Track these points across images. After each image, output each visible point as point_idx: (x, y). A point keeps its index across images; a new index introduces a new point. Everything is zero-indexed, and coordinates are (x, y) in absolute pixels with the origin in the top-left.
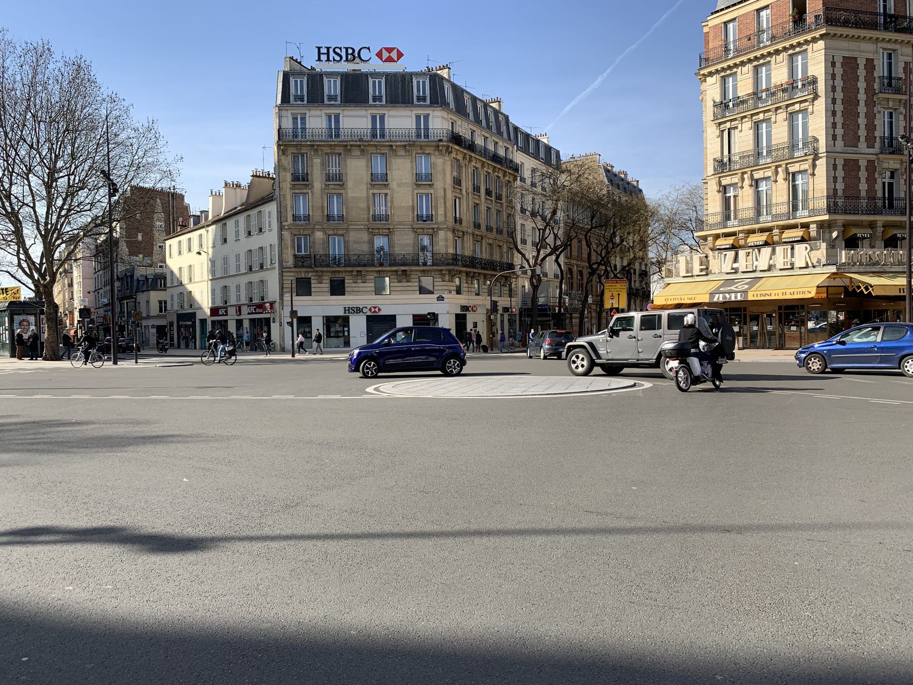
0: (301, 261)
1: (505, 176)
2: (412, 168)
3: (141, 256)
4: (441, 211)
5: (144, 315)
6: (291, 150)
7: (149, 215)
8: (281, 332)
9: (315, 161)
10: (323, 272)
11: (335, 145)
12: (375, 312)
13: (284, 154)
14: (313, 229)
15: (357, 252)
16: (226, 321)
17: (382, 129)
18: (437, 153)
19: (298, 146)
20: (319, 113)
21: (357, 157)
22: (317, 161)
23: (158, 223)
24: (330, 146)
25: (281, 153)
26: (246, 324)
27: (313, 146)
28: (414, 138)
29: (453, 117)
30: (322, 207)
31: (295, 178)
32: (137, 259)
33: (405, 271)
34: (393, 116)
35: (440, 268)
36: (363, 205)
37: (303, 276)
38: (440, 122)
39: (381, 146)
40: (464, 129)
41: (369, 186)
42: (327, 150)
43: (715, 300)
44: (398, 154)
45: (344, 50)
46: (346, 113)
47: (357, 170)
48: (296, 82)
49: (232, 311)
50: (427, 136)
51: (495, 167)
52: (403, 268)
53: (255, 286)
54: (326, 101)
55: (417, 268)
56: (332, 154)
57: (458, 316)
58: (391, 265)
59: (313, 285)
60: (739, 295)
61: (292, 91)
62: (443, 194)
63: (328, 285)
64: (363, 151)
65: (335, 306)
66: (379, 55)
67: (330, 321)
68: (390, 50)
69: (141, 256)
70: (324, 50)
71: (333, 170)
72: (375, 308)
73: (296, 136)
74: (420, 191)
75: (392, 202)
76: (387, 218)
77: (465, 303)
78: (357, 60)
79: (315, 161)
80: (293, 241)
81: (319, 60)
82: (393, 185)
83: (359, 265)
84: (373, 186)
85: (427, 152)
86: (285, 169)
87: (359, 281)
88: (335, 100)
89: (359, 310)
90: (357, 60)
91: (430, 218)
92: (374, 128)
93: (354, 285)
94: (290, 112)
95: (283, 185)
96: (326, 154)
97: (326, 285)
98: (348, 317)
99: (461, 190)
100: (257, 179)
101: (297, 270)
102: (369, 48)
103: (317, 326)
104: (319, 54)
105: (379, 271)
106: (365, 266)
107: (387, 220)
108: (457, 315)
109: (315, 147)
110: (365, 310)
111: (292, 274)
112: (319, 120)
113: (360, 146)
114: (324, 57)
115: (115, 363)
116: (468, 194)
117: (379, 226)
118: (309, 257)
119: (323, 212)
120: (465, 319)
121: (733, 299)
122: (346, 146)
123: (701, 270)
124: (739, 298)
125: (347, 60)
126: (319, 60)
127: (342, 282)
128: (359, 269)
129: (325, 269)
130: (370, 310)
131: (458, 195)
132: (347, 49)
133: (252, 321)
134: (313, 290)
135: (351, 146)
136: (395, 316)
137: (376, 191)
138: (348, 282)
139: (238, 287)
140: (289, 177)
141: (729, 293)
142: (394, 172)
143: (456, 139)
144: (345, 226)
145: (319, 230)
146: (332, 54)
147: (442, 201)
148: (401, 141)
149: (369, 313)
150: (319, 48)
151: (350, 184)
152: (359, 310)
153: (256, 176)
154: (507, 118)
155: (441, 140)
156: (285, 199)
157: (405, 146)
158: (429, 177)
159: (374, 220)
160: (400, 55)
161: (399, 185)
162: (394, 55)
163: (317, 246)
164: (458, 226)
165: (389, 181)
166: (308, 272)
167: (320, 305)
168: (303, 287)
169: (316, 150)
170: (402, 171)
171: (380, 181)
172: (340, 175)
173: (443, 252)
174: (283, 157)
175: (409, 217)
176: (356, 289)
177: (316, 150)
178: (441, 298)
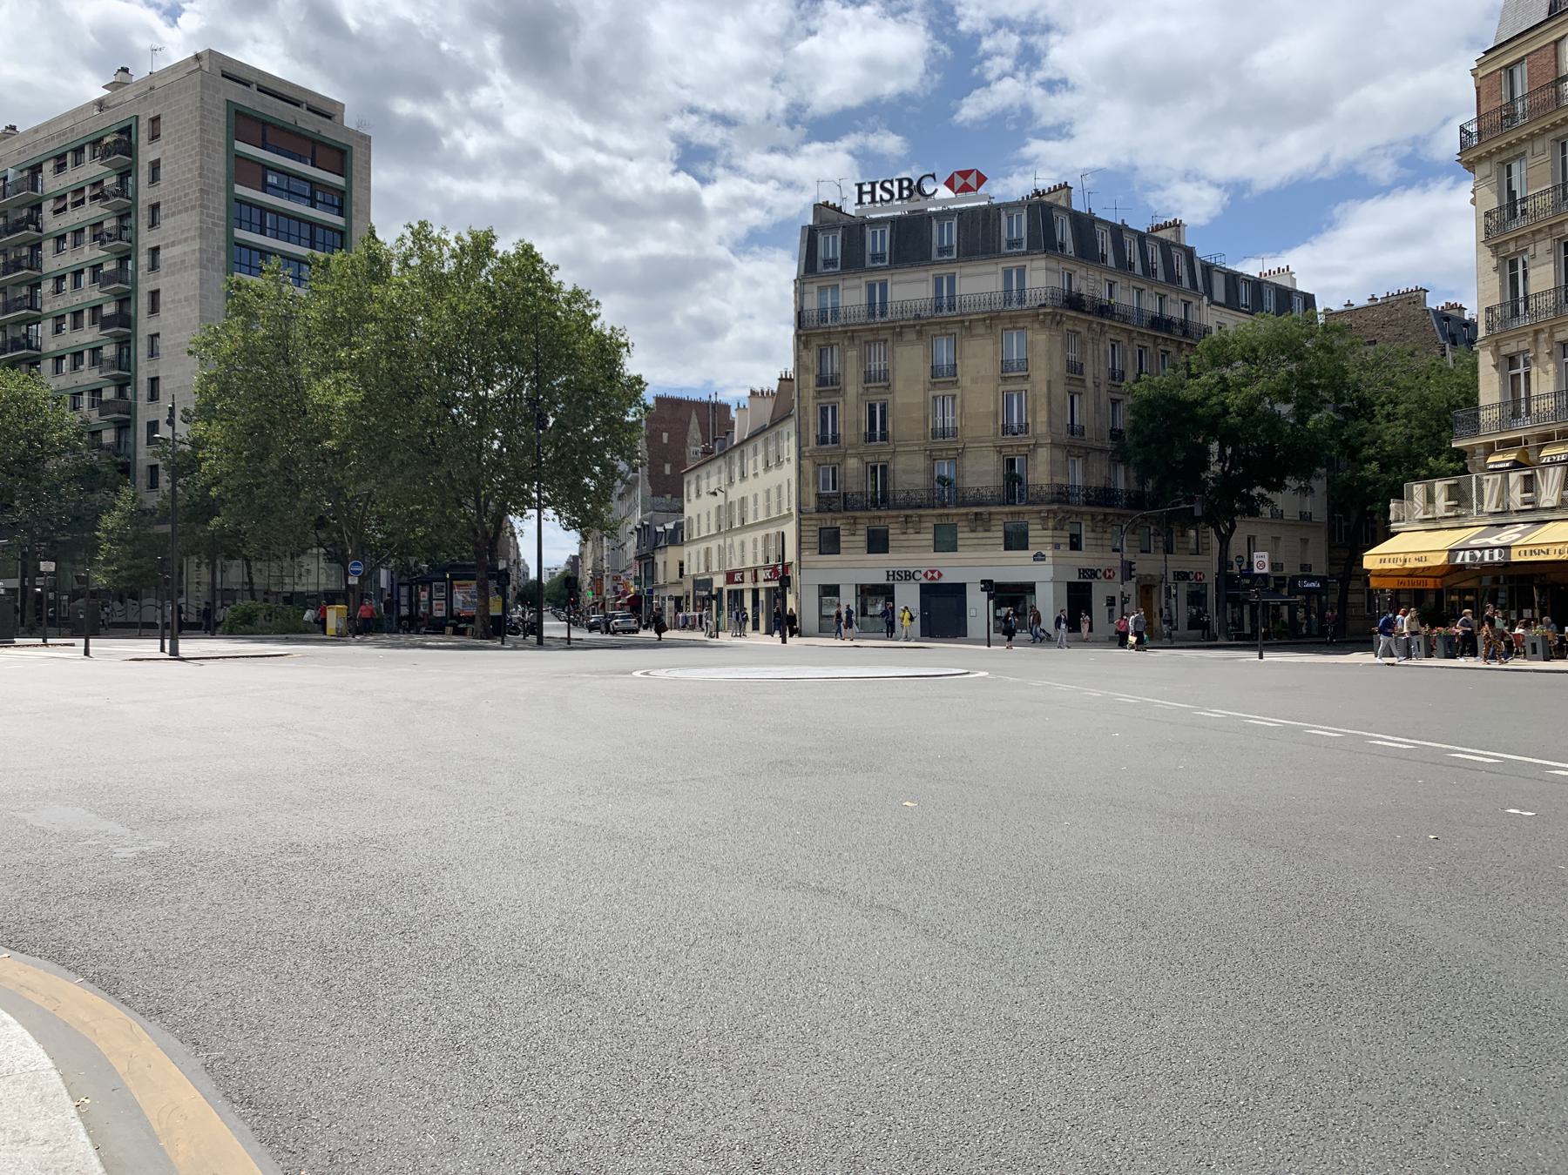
0: (825, 504)
1: (1180, 350)
3: (668, 496)
4: (1042, 417)
5: (661, 582)
7: (680, 439)
14: (845, 455)
15: (907, 487)
16: (742, 591)
18: (1037, 326)
19: (828, 334)
20: (856, 282)
22: (852, 354)
23: (693, 449)
26: (762, 596)
28: (999, 307)
29: (1067, 266)
30: (858, 422)
31: (822, 381)
34: (967, 276)
35: (1036, 508)
38: (1040, 277)
40: (1089, 283)
43: (1458, 561)
45: (896, 184)
46: (896, 278)
47: (910, 364)
48: (874, 234)
49: (748, 576)
50: (1021, 301)
52: (976, 510)
54: (868, 263)
55: (931, 512)
56: (875, 341)
57: (1072, 587)
58: (958, 505)
60: (1496, 551)
61: (821, 253)
62: (1045, 389)
63: (864, 538)
64: (920, 333)
65: (874, 570)
66: (950, 184)
67: (867, 592)
68: (965, 174)
69: (668, 496)
70: (867, 188)
71: (876, 365)
73: (873, 315)
74: (1009, 388)
75: (962, 407)
77: (1085, 564)
78: (916, 195)
80: (816, 474)
81: (860, 202)
82: (965, 380)
83: (908, 507)
84: (1005, 379)
88: (883, 260)
89: (908, 576)
90: (916, 195)
91: (1024, 428)
92: (939, 297)
95: (804, 392)
97: (861, 539)
98: (893, 586)
99: (1083, 381)
102: (933, 176)
103: (848, 599)
104: (861, 193)
106: (920, 507)
109: (851, 334)
110: (917, 576)
114: (867, 198)
116: (1097, 386)
117: (946, 446)
119: (858, 428)
121: (1487, 559)
123: (1449, 509)
124: (1496, 558)
125: (901, 197)
126: (860, 202)
129: (858, 514)
132: (900, 181)
133: (768, 590)
136: (837, 587)
137: (938, 393)
138: (894, 533)
141: (1480, 549)
143: (1074, 302)
144: (890, 448)
146: (879, 192)
147: (1044, 400)
149: (924, 581)
150: (860, 186)
151: (899, 385)
152: (908, 576)
154: (1190, 253)
156: (806, 413)
159: (934, 436)
160: (981, 179)
161: (974, 381)
162: (972, 181)
168: (829, 543)
170: (978, 359)
174: (804, 353)
175: (989, 429)
177: (852, 338)
178: (1039, 557)
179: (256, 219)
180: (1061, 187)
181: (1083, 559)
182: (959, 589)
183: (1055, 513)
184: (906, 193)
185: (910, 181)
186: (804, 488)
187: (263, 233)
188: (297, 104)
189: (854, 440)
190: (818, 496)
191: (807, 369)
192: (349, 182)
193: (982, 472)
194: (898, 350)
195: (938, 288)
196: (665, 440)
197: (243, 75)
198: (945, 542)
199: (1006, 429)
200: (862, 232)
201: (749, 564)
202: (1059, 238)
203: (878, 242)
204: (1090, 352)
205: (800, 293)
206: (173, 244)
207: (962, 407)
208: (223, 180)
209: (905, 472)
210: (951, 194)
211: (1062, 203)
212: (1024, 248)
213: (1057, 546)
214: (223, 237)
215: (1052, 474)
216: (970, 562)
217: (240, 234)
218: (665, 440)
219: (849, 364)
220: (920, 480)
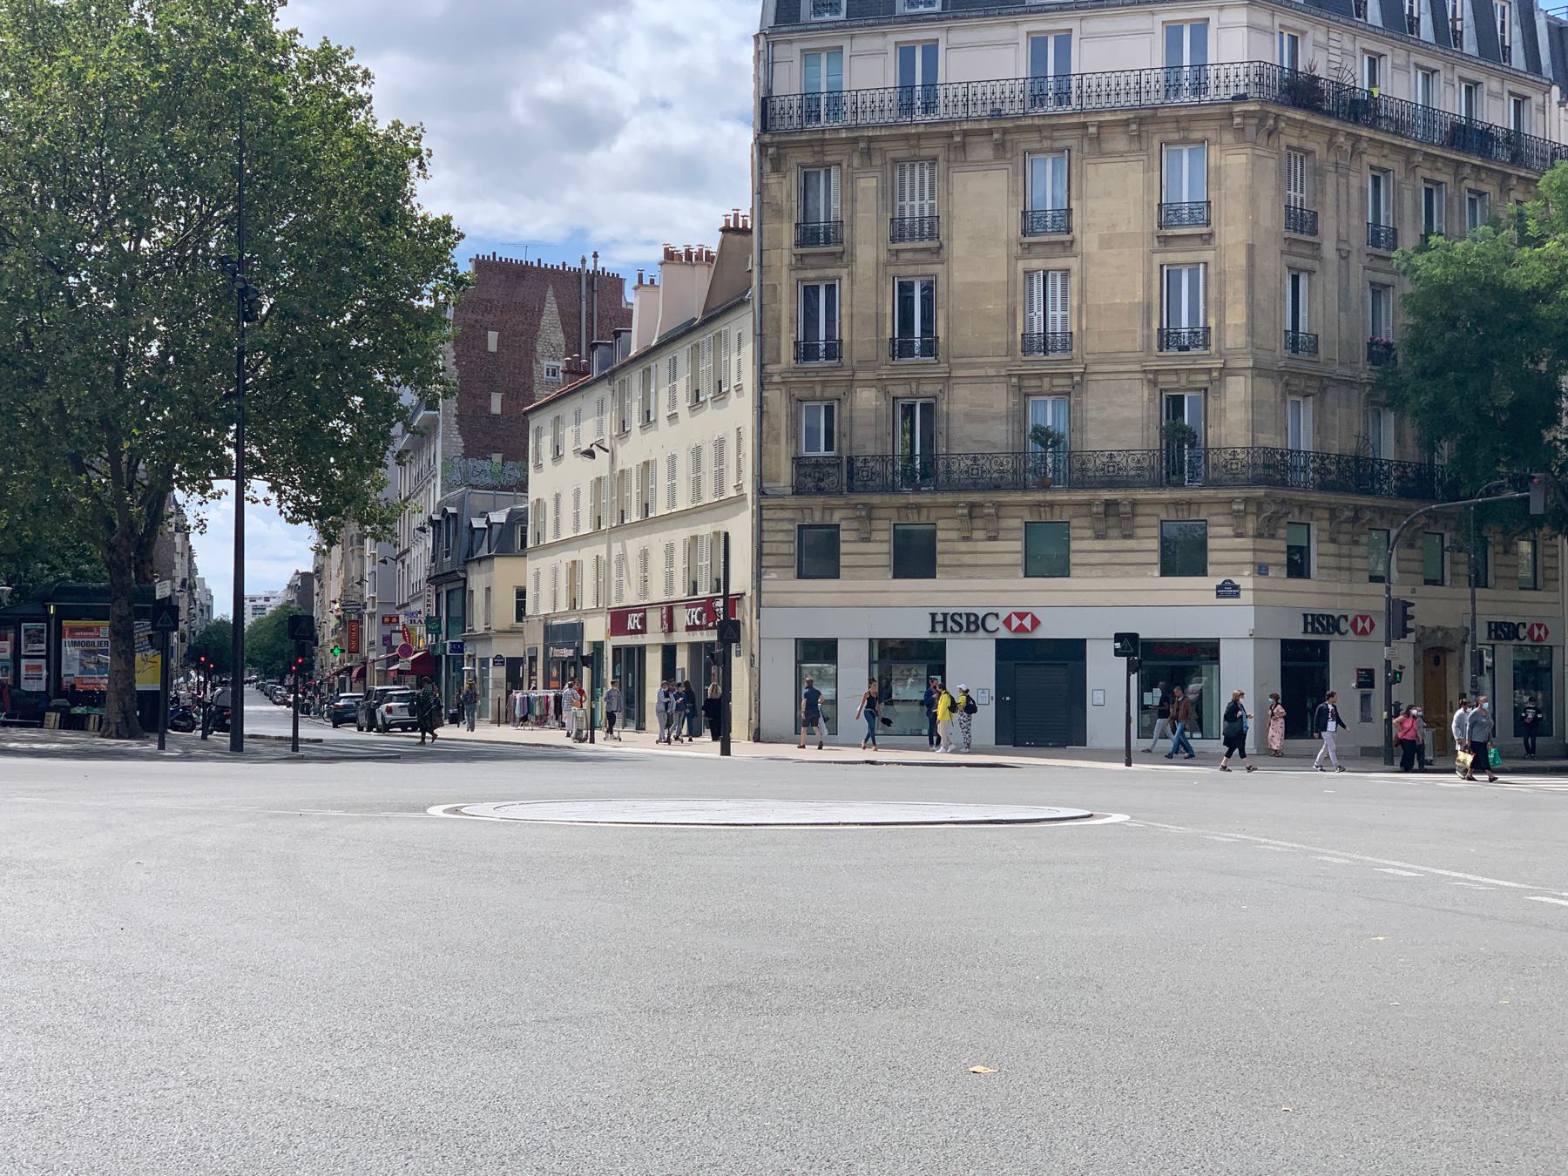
2: (1148, 188)
3: (497, 458)
4: (1236, 316)
5: (479, 627)
6: (796, 158)
8: (759, 680)
9: (862, 183)
10: (999, 505)
11: (919, 136)
12: (1021, 628)
13: (776, 169)
14: (851, 383)
15: (974, 448)
16: (642, 649)
17: (1063, 75)
18: (1228, 137)
19: (820, 144)
20: (875, 43)
21: (983, 166)
22: (868, 184)
24: (907, 137)
25: (768, 167)
27: (856, 140)
28: (1154, 99)
29: (1290, 21)
30: (879, 318)
32: (486, 465)
33: (1115, 503)
35: (1224, 494)
36: (996, 306)
37: (817, 519)
39: (1054, 128)
41: (1017, 250)
42: (901, 151)
44: (1106, 147)
46: (957, 37)
47: (980, 204)
49: (654, 619)
50: (1199, 87)
51: (1459, 164)
52: (1107, 495)
53: (705, 549)
56: (913, 161)
57: (1290, 649)
58: (1072, 486)
59: (844, 548)
65: (906, 610)
67: (892, 655)
69: (497, 458)
71: (915, 206)
72: (1021, 616)
74: (1172, 257)
75: (1082, 293)
76: (1067, 342)
79: (862, 183)
80: (794, 418)
82: (1088, 241)
83: (976, 486)
84: (1165, 240)
85: (1197, 135)
86: (778, 213)
87: (1114, 532)
89: (974, 624)
93: (963, 546)
94: (797, 47)
95: (772, 257)
96: (895, 161)
97: (881, 548)
99: (1317, 246)
100: (737, 238)
101: (804, 501)
105: (1039, 505)
106: (997, 488)
107: (1066, 346)
109: (865, 146)
110: (991, 624)
111: (787, 514)
112: (1009, 52)
113: (990, 132)
115: (1129, 764)
116: (1344, 256)
117: (1049, 369)
118: (836, 463)
119: (879, 330)
120: (1325, 657)
122: (950, 135)
127: (1062, 532)
128: (976, 497)
130: (1008, 622)
131: (1301, 262)
134: (844, 560)
135: (966, 133)
136: (836, 640)
137: (1036, 264)
138: (946, 538)
139: (670, 549)
140: (787, 234)
142: (1092, 204)
143: (1301, 92)
145: (866, 383)
148: (1113, 110)
149: (1004, 634)
151: (959, 246)
153: (736, 230)
155: (1242, 98)
157: (1127, 123)
158: (1203, 212)
161: (1106, 243)
163: (859, 431)
164: (1303, 362)
165: (1076, 232)
166: (832, 509)
167: (869, 604)
168: (819, 556)
169: (868, 154)
170: (1114, 199)
171: (1045, 231)
172: (934, 219)
174: (773, 180)
176: (967, 559)
177: (868, 154)
178: (1228, 590)
183: (1259, 503)
189: (870, 352)
190: (798, 461)
193: (1119, 421)
194: (957, 178)
198: (1047, 557)
199: (1168, 338)
201: (657, 595)
205: (767, 63)
207: (1082, 293)
209: (970, 417)
213: (1261, 570)
215: (1255, 427)
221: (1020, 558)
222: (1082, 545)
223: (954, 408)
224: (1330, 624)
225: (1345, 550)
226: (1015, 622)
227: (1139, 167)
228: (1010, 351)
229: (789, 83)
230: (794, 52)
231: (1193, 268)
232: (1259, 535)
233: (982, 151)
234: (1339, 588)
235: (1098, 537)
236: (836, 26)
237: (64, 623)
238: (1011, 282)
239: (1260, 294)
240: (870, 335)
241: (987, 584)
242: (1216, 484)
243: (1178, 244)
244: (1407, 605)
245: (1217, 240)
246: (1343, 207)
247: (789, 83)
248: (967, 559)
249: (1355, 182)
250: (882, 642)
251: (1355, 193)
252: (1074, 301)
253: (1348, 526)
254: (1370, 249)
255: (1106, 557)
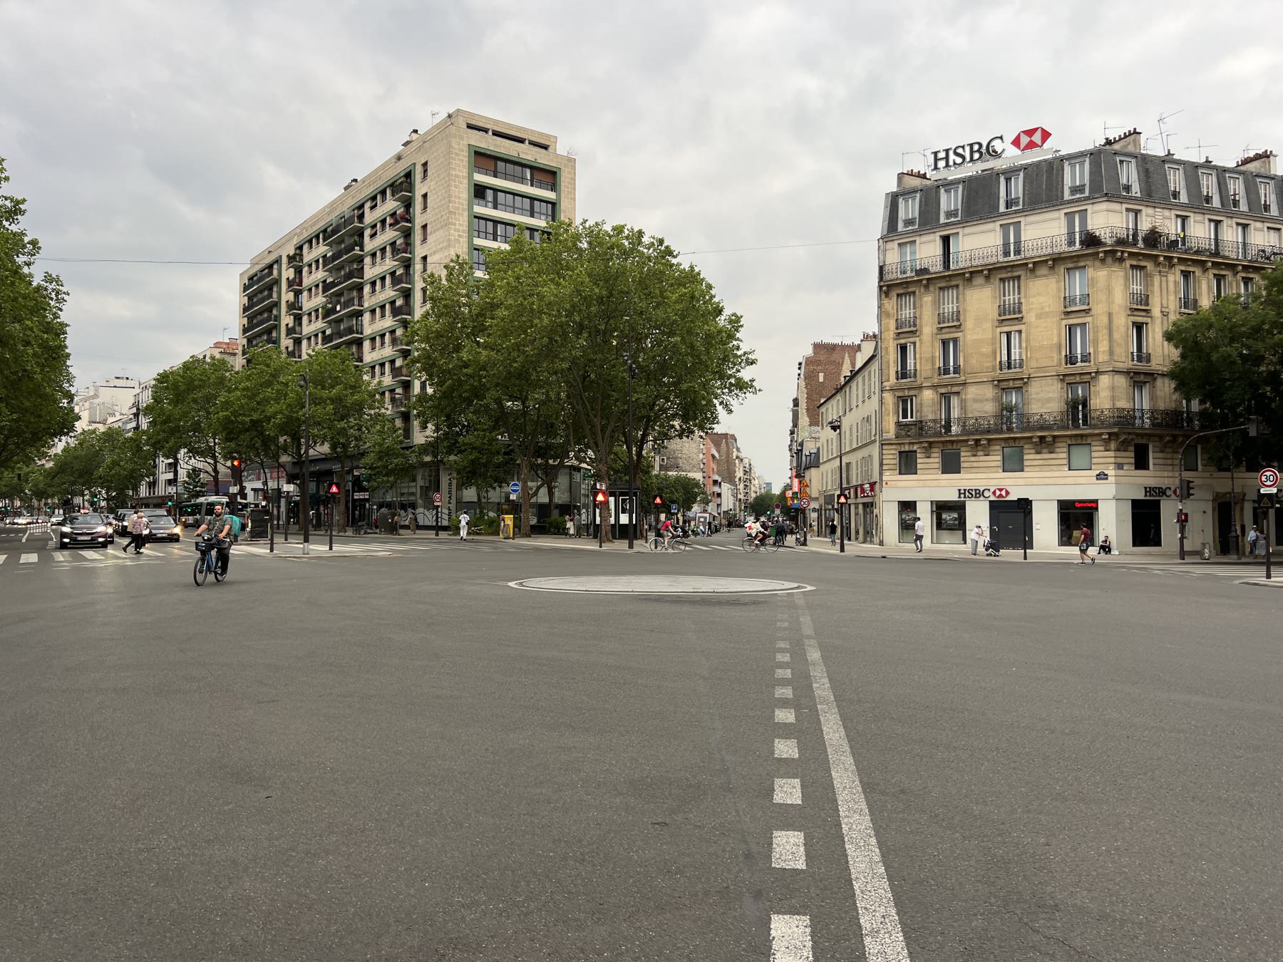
2: (1059, 290)
12: (1001, 496)
15: (977, 414)
18: (1098, 263)
30: (933, 358)
36: (987, 349)
45: (967, 149)
47: (980, 303)
56: (905, 294)
61: (902, 215)
62: (1106, 320)
65: (947, 488)
66: (1016, 142)
67: (940, 508)
68: (1030, 133)
72: (1001, 490)
75: (1028, 340)
77: (1152, 482)
81: (936, 168)
82: (1030, 317)
86: (888, 315)
88: (956, 215)
89: (978, 494)
93: (973, 459)
102: (1001, 138)
104: (936, 160)
107: (1021, 366)
108: (1133, 501)
110: (986, 494)
112: (1056, 223)
114: (941, 164)
126: (936, 168)
130: (994, 493)
132: (971, 145)
134: (963, 465)
146: (952, 157)
147: (1106, 332)
149: (993, 498)
150: (936, 154)
151: (969, 324)
152: (978, 494)
160: (1046, 135)
161: (1039, 317)
162: (1037, 138)
167: (930, 485)
168: (907, 464)
170: (1042, 297)
171: (1010, 315)
173: (1107, 405)
174: (886, 301)
176: (975, 464)
178: (1102, 476)
179: (490, 230)
180: (1130, 134)
181: (1151, 477)
182: (1024, 506)
183: (1116, 435)
184: (976, 156)
185: (980, 145)
186: (885, 418)
187: (495, 239)
188: (521, 141)
189: (929, 374)
190: (898, 424)
191: (888, 315)
192: (559, 196)
193: (1046, 400)
194: (1031, 284)
195: (1071, 225)
196: (821, 379)
197: (481, 124)
198: (1013, 464)
199: (1071, 360)
200: (938, 193)
201: (854, 483)
202: (1124, 181)
203: (949, 202)
204: (1157, 283)
205: (882, 251)
206: (434, 253)
207: (1028, 340)
208: (466, 203)
209: (975, 401)
210: (1018, 152)
211: (1131, 149)
212: (1087, 194)
213: (1119, 466)
214: (466, 245)
215: (1113, 399)
216: (1035, 481)
217: (478, 242)
218: (821, 379)
219: (927, 308)
220: (989, 408)
221: (1000, 464)
222: (965, 456)
223: (969, 396)
224: (1162, 492)
225: (1169, 456)
226: (998, 493)
227: (1054, 280)
228: (994, 369)
229: (893, 257)
230: (894, 245)
231: (1020, 332)
232: (1118, 450)
233: (979, 280)
234: (1166, 474)
235: (1038, 453)
236: (959, 223)
237: (944, 516)
238: (994, 338)
239: (1116, 336)
240: (929, 366)
241: (986, 477)
242: (1095, 427)
243: (1073, 315)
244: (1189, 482)
245: (1093, 312)
246: (1164, 291)
247: (893, 257)
248: (975, 464)
249: (1171, 278)
250: (937, 502)
251: (1171, 286)
252: (1024, 345)
253: (1168, 445)
254: (1183, 310)
255: (1041, 462)
